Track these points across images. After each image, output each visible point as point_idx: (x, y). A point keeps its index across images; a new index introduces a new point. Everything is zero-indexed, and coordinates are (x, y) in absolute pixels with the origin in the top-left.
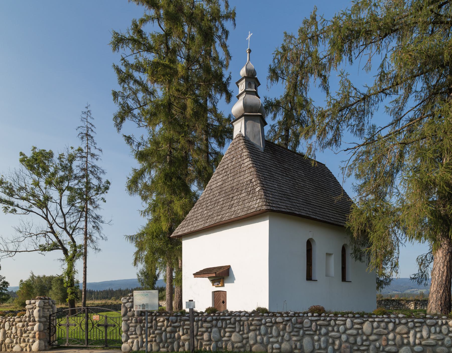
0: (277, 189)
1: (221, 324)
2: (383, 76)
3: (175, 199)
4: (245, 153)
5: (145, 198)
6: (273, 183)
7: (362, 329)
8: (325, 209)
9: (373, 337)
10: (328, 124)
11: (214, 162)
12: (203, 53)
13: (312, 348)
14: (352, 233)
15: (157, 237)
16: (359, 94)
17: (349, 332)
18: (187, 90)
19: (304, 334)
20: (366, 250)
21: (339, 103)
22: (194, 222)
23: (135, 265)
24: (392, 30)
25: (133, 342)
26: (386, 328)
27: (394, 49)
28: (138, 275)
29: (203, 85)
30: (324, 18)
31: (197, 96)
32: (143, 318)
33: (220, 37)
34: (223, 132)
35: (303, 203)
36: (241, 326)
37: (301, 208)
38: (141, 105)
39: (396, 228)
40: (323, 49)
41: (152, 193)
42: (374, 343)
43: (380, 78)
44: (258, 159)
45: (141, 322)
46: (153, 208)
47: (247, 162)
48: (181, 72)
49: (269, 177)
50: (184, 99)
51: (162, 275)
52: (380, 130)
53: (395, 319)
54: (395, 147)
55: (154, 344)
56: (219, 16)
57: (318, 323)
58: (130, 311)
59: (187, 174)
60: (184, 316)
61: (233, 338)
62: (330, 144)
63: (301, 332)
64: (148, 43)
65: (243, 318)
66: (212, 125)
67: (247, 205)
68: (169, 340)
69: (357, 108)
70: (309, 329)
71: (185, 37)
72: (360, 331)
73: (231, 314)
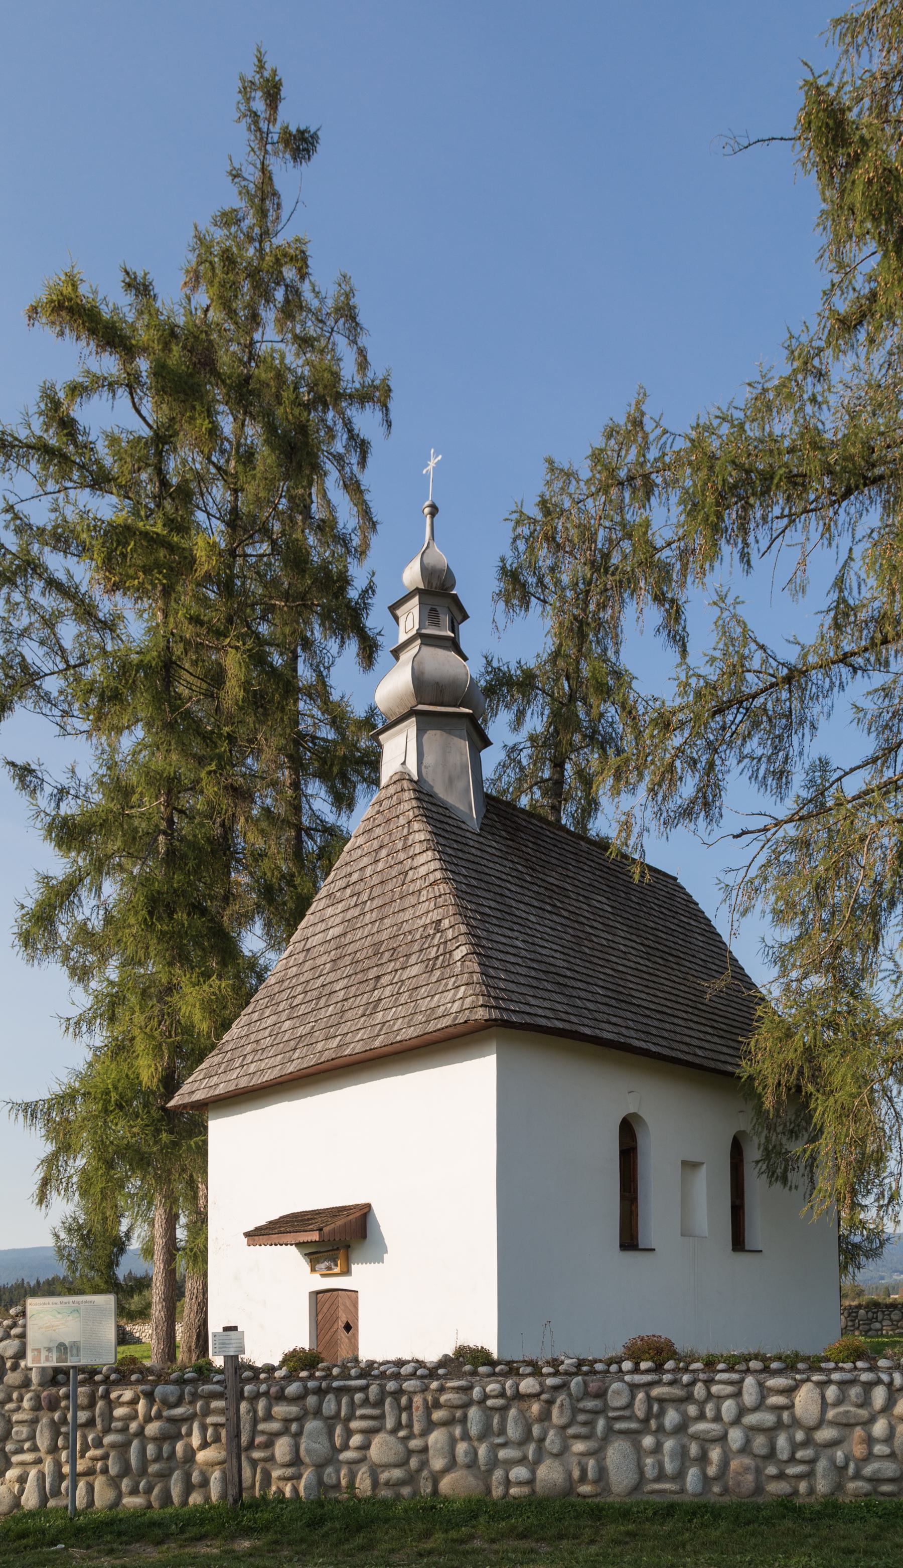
0: (523, 953)
1: (333, 1406)
2: (842, 614)
3: (184, 979)
4: (420, 834)
5: (81, 974)
6: (510, 933)
7: (790, 1407)
8: (676, 1021)
9: (825, 1434)
10: (680, 750)
11: (319, 857)
12: (283, 505)
13: (636, 1476)
14: (760, 1096)
15: (120, 1107)
16: (774, 664)
17: (751, 1419)
18: (230, 620)
19: (609, 1431)
20: (805, 1151)
21: (715, 688)
22: (249, 1058)
23: (41, 1202)
24: (865, 478)
25: (22, 1480)
26: (866, 1402)
27: (875, 535)
28: (58, 1237)
29: (281, 609)
30: (665, 423)
31: (260, 640)
32: (62, 1391)
33: (339, 459)
34: (350, 764)
35: (607, 1000)
36: (401, 1410)
37: (599, 1016)
38: (72, 662)
39: (891, 1081)
40: (665, 518)
41: (104, 959)
42: (829, 1451)
43: (835, 619)
44: (460, 854)
45: (53, 1406)
46: (110, 1008)
47: (427, 864)
48: (205, 563)
49: (499, 914)
50: (218, 650)
51: (140, 1233)
52: (840, 779)
53: (891, 1374)
54: (884, 831)
55: (99, 1482)
56: (337, 392)
57: (656, 1392)
58: (15, 1367)
59: (227, 898)
60: (207, 1381)
61: (376, 1452)
62: (687, 813)
63: (601, 1424)
64: (97, 462)
65: (408, 1385)
66: (314, 738)
67: (424, 1004)
68: (153, 1468)
69: (770, 705)
70: (627, 1413)
71: (223, 452)
72: (785, 1415)
73: (369, 1370)
